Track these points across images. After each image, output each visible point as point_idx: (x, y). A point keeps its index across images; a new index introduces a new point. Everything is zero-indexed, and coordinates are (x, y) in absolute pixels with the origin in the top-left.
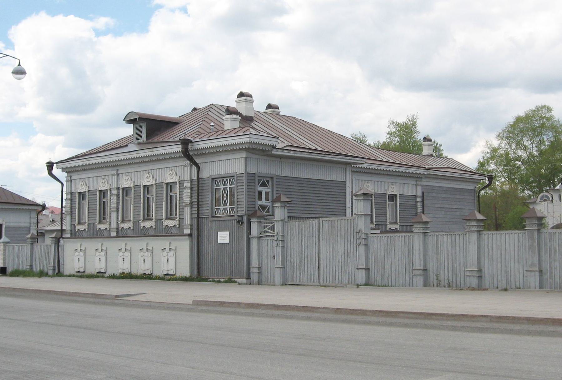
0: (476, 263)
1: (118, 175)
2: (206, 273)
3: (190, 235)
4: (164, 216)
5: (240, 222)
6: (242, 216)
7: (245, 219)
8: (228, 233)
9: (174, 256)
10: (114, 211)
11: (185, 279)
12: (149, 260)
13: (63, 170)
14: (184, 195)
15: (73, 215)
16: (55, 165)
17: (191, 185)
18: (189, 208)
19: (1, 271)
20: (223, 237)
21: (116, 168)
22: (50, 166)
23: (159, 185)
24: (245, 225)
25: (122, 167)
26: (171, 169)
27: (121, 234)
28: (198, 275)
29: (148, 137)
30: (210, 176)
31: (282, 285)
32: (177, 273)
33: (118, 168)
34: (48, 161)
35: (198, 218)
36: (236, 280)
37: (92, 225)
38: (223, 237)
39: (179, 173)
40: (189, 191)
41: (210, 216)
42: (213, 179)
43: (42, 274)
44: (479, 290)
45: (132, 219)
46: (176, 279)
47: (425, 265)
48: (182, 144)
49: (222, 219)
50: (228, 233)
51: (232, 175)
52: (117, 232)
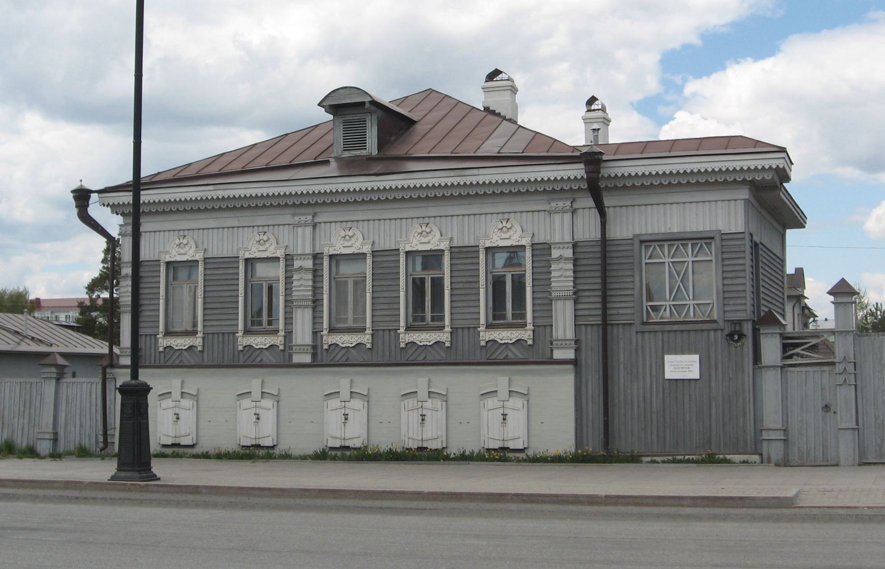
0: (51, 426)
1: (314, 226)
2: (623, 443)
3: (575, 362)
4: (241, 326)
5: (735, 335)
6: (739, 322)
7: (747, 329)
8: (696, 357)
9: (540, 409)
10: (566, 298)
11: (558, 459)
12: (269, 418)
13: (115, 208)
14: (295, 283)
15: (318, 309)
16: (94, 197)
17: (314, 264)
18: (570, 305)
19: (8, 450)
20: (683, 366)
21: (310, 210)
22: (82, 196)
23: (458, 252)
24: (748, 342)
25: (325, 209)
26: (182, 233)
27: (323, 359)
28: (602, 446)
29: (382, 143)
30: (636, 236)
31: (860, 465)
32: (450, 445)
33: (317, 210)
34: (76, 185)
35: (605, 326)
36: (728, 457)
37: (384, 332)
38: (683, 366)
39: (566, 227)
40: (571, 266)
41: (637, 322)
42: (642, 242)
43: (31, 453)
44: (785, 466)
45: (368, 324)
46: (536, 460)
47: (786, 421)
48: (587, 164)
49: (676, 327)
50: (696, 357)
51: (711, 235)
52: (314, 355)
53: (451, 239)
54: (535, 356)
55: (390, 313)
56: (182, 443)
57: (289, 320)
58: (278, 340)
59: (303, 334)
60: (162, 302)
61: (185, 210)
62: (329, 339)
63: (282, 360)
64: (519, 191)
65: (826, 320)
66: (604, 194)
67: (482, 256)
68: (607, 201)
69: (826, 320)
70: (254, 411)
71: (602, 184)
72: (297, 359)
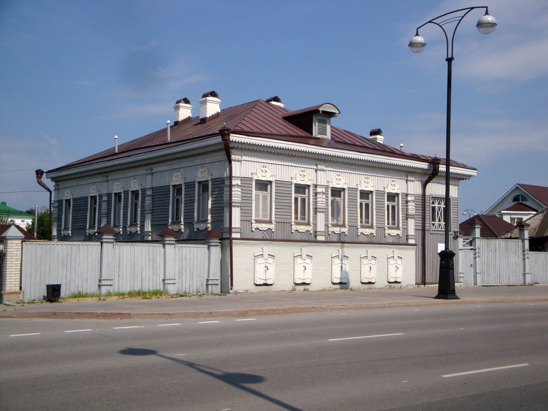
53: (212, 174)
54: (401, 243)
55: (353, 218)
56: (269, 283)
57: (315, 219)
58: (310, 228)
59: (321, 227)
60: (254, 202)
61: (305, 157)
62: (331, 229)
63: (311, 239)
64: (264, 151)
65: (53, 292)
66: (233, 151)
67: (171, 190)
68: (451, 182)
69: (53, 292)
70: (303, 265)
71: (231, 145)
72: (319, 238)
